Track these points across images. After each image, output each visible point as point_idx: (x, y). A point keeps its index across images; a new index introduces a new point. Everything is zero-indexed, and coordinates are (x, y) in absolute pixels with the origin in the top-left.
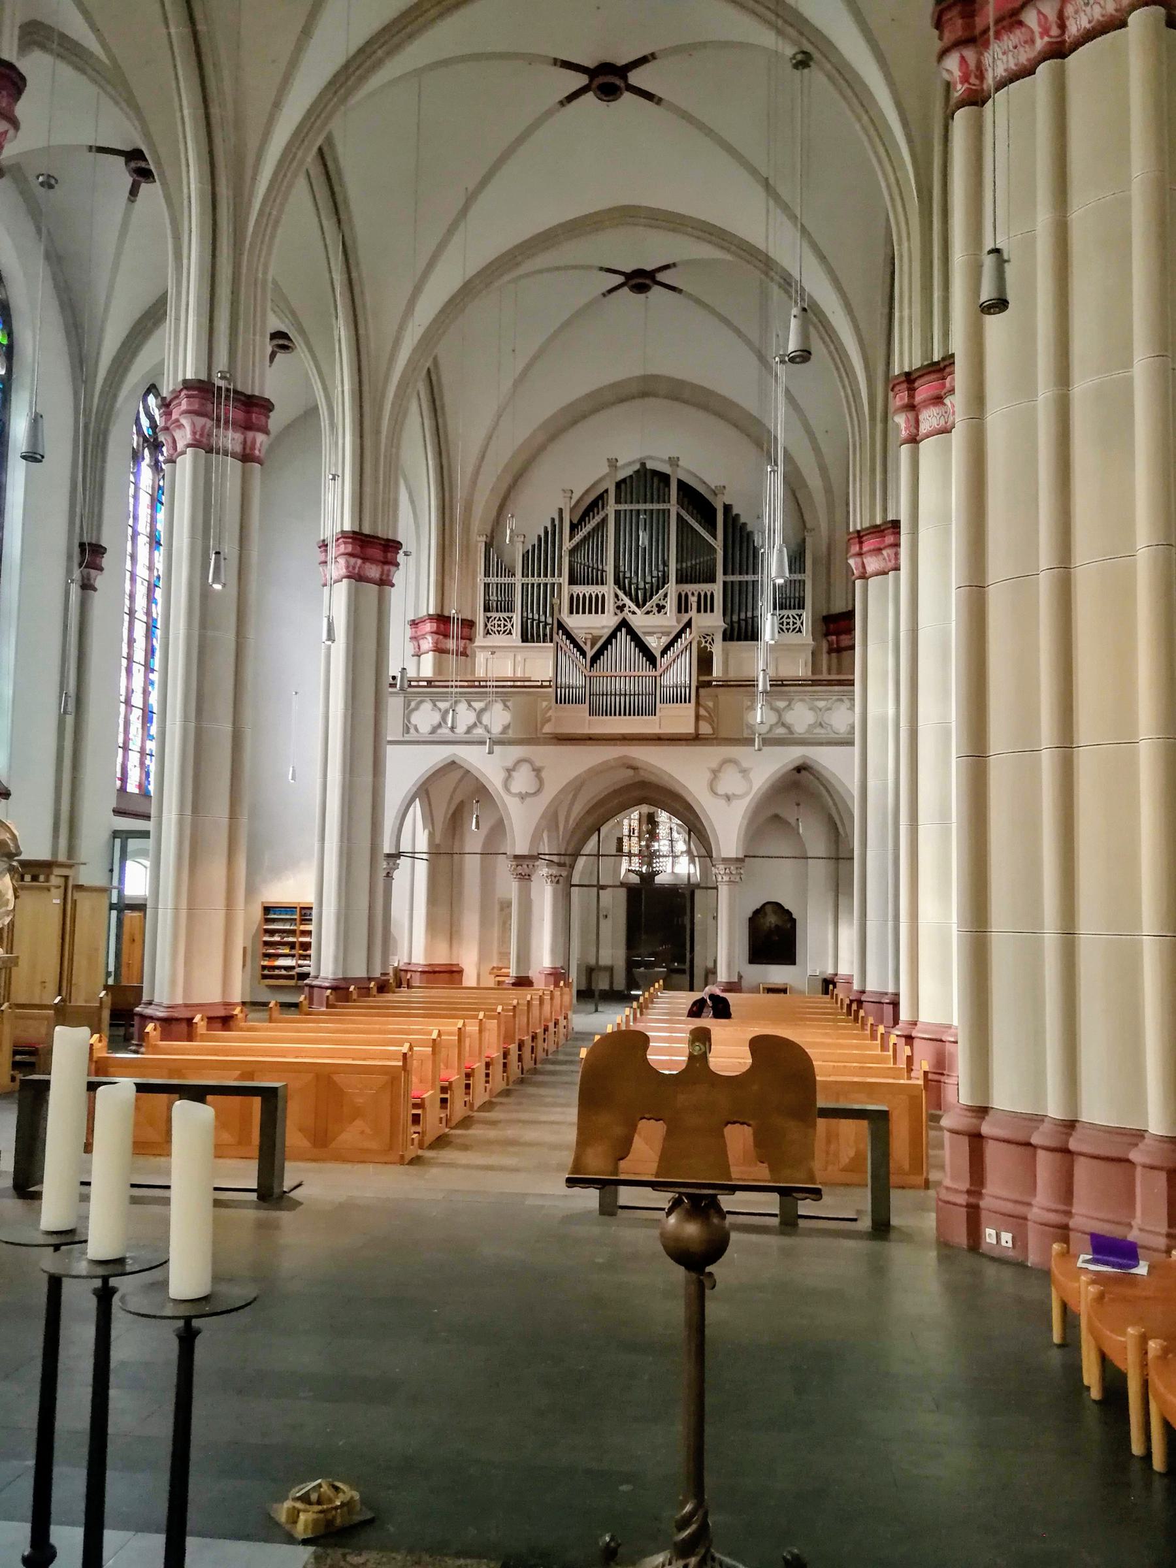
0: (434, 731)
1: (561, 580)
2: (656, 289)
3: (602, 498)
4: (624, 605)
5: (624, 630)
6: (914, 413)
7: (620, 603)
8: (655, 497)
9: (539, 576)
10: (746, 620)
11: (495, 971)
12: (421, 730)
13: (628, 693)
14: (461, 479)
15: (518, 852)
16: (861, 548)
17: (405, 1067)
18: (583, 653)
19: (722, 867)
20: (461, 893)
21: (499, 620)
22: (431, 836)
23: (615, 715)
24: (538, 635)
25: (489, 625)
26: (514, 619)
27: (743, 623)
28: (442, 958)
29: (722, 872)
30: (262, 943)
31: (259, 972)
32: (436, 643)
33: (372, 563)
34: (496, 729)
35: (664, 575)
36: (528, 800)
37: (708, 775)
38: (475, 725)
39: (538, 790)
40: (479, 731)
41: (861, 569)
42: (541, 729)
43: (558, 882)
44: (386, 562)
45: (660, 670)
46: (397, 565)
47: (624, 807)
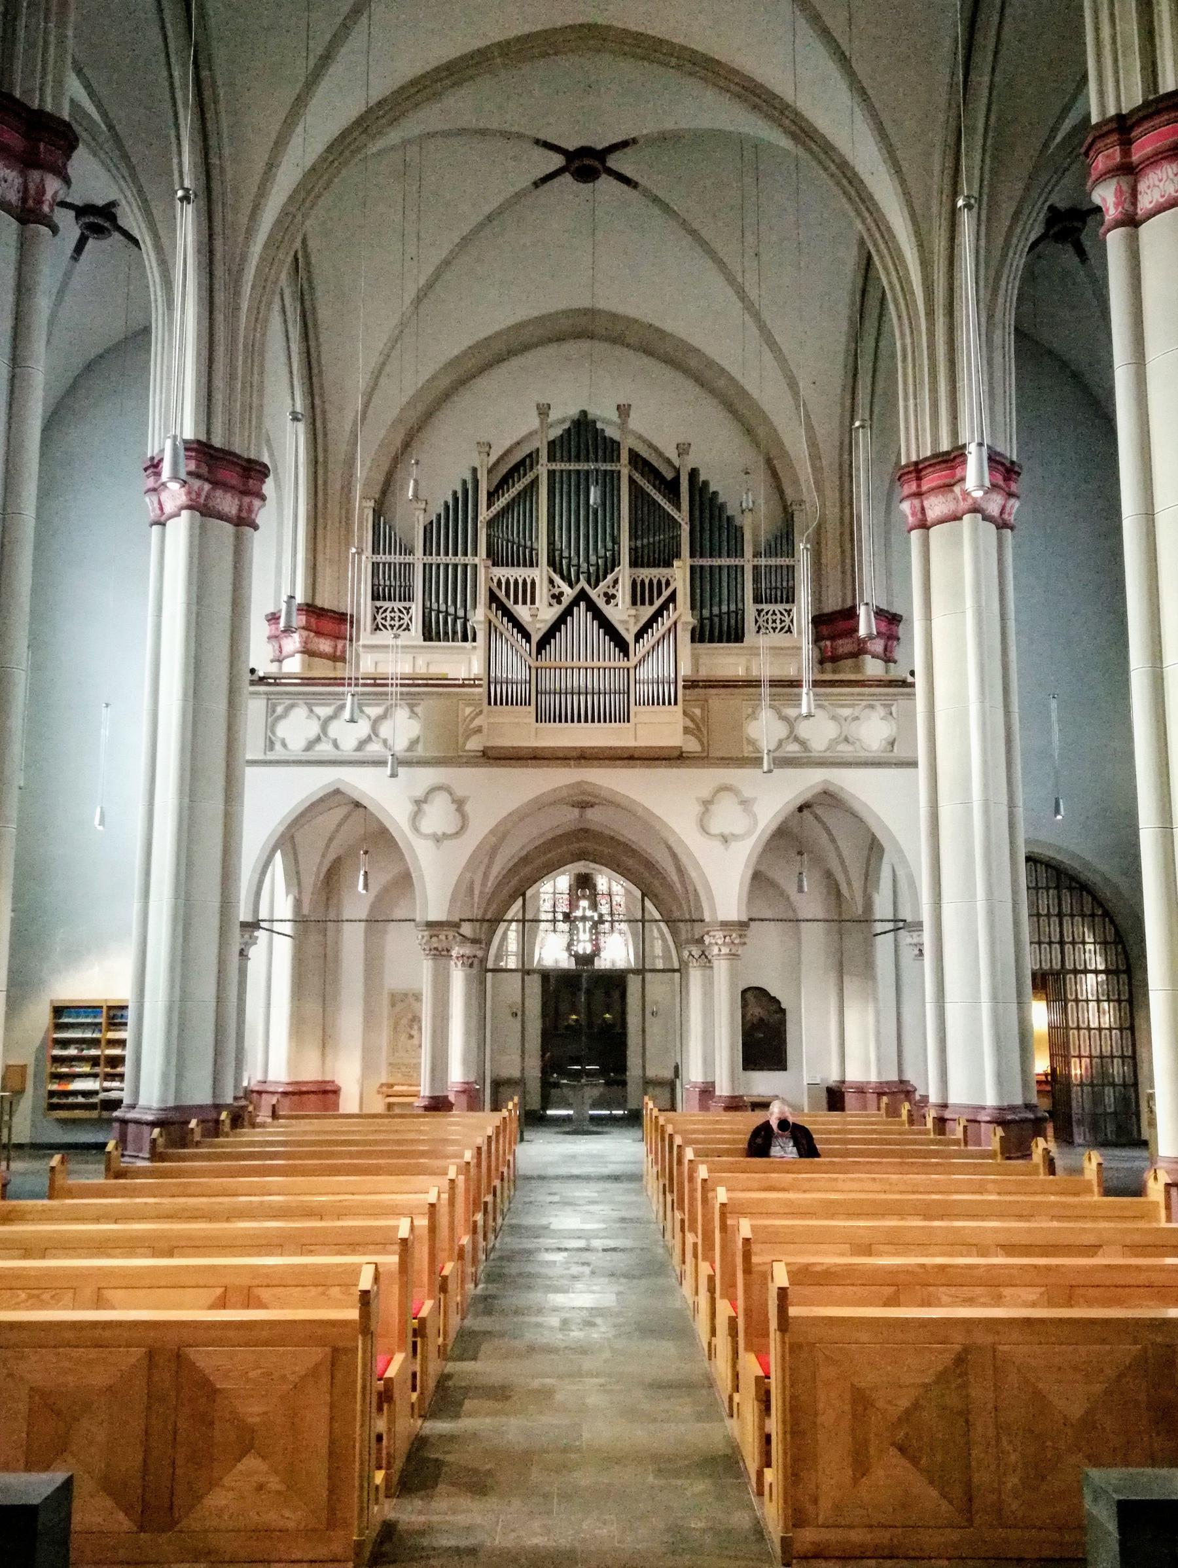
0: (310, 746)
1: (477, 560)
2: (604, 177)
3: (531, 460)
4: (561, 594)
5: (582, 604)
6: (1131, 178)
7: (556, 591)
8: (600, 453)
9: (447, 554)
10: (720, 615)
11: (385, 1089)
12: (290, 746)
13: (590, 690)
14: (342, 422)
15: (433, 916)
16: (919, 486)
17: (365, 1325)
18: (527, 636)
19: (721, 934)
20: (336, 981)
21: (393, 611)
22: (298, 904)
23: (566, 721)
24: (446, 633)
25: (379, 618)
26: (413, 611)
27: (716, 620)
28: (310, 1073)
29: (720, 942)
30: (50, 1059)
31: (44, 1104)
32: (306, 642)
33: (226, 492)
34: (400, 745)
35: (613, 555)
36: (447, 843)
37: (697, 808)
38: (318, 739)
39: (462, 828)
40: (374, 748)
41: (919, 516)
42: (464, 744)
43: (471, 965)
44: (245, 492)
45: (634, 660)
46: (263, 498)
47: (549, 868)
